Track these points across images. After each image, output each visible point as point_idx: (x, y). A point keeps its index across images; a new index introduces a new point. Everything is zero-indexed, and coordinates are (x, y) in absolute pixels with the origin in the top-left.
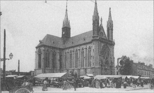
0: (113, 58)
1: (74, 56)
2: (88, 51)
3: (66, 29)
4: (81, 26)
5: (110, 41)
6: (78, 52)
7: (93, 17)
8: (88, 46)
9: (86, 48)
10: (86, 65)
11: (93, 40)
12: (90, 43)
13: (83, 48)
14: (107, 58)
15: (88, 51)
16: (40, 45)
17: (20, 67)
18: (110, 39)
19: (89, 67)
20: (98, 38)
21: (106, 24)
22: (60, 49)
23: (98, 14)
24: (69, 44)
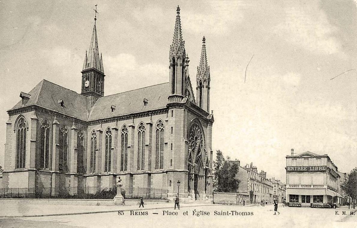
0: (209, 152)
1: (117, 143)
2: (154, 130)
3: (95, 76)
4: (136, 72)
5: (202, 111)
6: (113, 136)
7: (172, 49)
8: (155, 119)
9: (151, 125)
10: (132, 166)
11: (169, 106)
12: (164, 111)
13: (109, 129)
14: (199, 152)
15: (154, 130)
16: (23, 106)
17: (86, 212)
18: (204, 108)
19: (140, 171)
20: (183, 101)
21: (196, 72)
22: (77, 121)
23: (182, 43)
24: (98, 110)
